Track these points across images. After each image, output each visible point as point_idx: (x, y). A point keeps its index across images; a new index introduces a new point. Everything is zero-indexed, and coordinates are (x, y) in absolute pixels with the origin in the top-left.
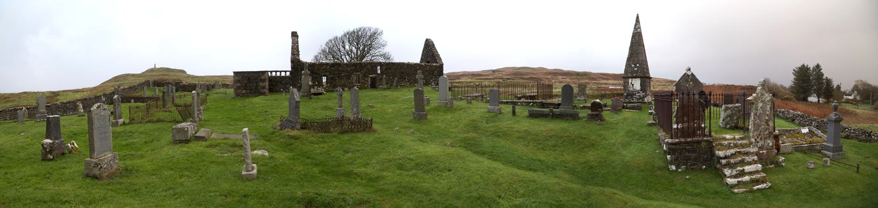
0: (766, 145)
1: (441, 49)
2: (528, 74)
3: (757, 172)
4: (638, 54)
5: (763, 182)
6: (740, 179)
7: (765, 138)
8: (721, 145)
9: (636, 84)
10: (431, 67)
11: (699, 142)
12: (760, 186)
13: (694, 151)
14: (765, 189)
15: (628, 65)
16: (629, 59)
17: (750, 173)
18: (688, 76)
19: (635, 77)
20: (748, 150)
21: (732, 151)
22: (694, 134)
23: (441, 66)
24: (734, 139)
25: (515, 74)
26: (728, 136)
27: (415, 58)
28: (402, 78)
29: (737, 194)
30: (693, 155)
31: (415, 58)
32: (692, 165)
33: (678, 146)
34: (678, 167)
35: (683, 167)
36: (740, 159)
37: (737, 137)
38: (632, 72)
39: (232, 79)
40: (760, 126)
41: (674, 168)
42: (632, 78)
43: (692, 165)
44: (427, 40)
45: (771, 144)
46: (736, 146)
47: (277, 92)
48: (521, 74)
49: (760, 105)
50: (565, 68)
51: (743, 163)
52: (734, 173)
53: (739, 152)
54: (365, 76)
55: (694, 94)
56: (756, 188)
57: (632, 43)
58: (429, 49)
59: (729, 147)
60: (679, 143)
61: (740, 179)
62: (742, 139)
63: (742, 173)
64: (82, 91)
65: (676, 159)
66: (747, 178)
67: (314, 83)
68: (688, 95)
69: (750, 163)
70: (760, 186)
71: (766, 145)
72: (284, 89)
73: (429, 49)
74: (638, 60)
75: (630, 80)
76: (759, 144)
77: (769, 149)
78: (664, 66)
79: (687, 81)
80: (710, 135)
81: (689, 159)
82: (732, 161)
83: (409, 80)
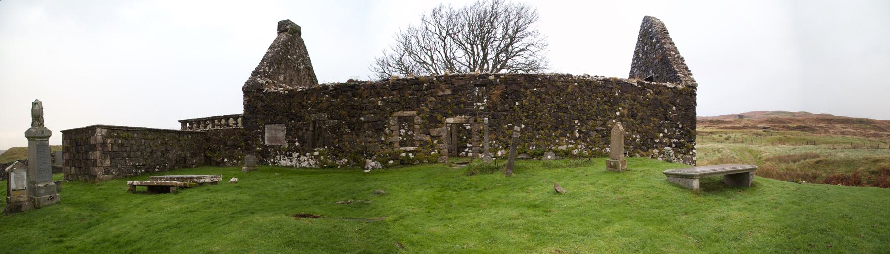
1: (686, 43)
2: (791, 121)
10: (658, 91)
23: (690, 92)
25: (772, 121)
27: (615, 62)
28: (562, 127)
31: (615, 62)
44: (647, 20)
47: (218, 164)
48: (781, 121)
50: (837, 113)
54: (433, 121)
58: (655, 48)
64: (785, 113)
67: (291, 142)
72: (231, 158)
73: (655, 48)
78: (57, 126)
83: (585, 136)
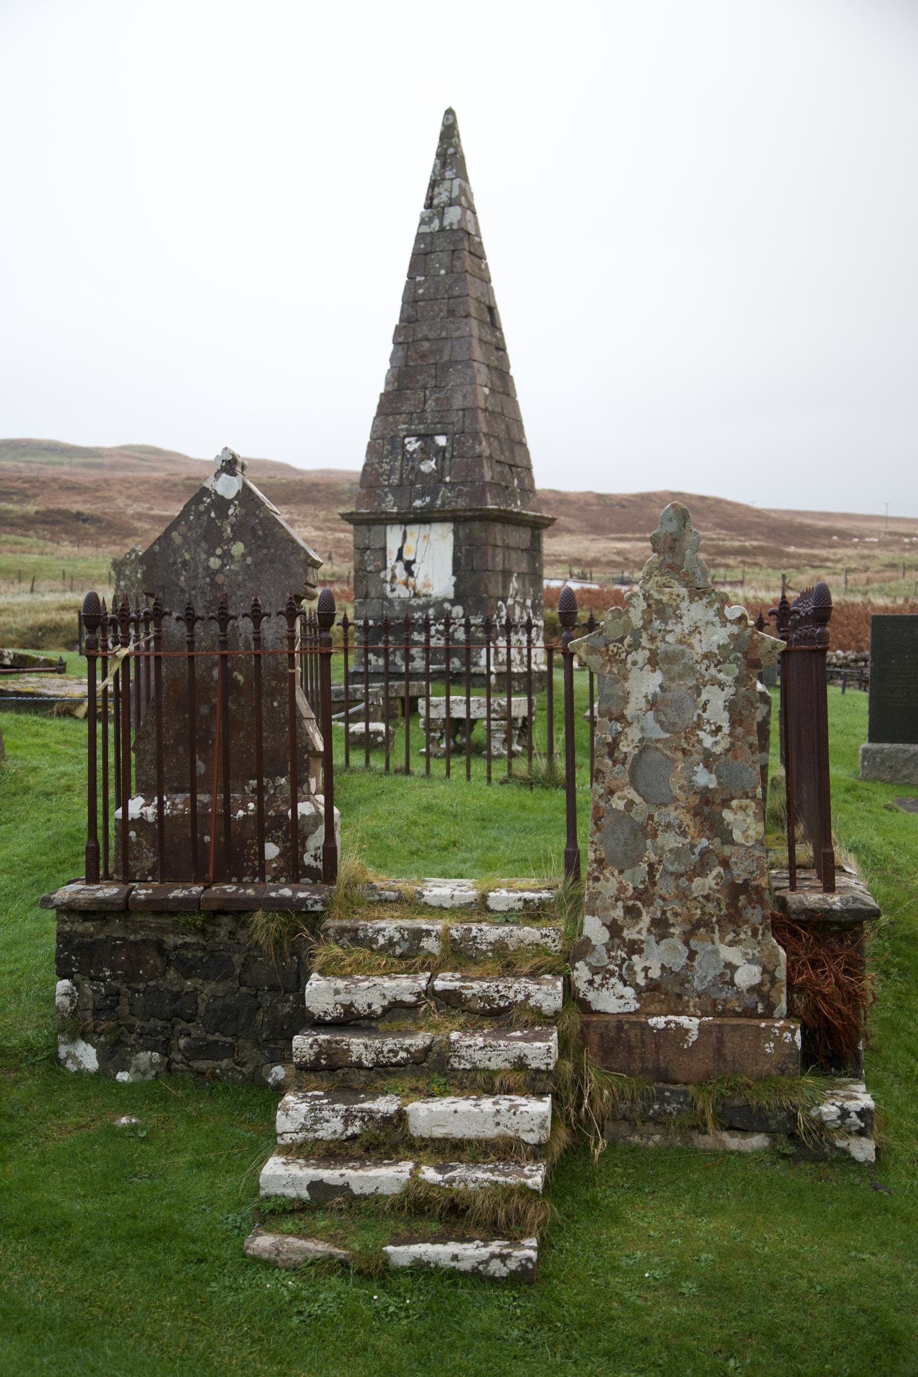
0: (704, 974)
2: (37, 486)
3: (504, 1150)
4: (443, 369)
5: (493, 1229)
6: (330, 1175)
7: (694, 929)
8: (355, 938)
9: (429, 561)
11: (239, 911)
12: (440, 1252)
13: (214, 965)
14: (477, 1277)
15: (384, 442)
16: (389, 405)
17: (449, 1150)
18: (221, 504)
19: (425, 518)
20: (517, 989)
21: (404, 986)
22: (236, 858)
24: (480, 908)
26: (441, 890)
29: (268, 1264)
30: (208, 991)
32: (199, 1051)
33: (116, 929)
34: (113, 1056)
35: (145, 1057)
36: (420, 1040)
37: (502, 897)
38: (403, 489)
39: (357, 479)
40: (646, 831)
41: (87, 1056)
42: (408, 519)
43: (199, 1051)
45: (747, 975)
46: (459, 954)
49: (646, 683)
51: (434, 1071)
52: (332, 1127)
53: (451, 1001)
55: (257, 615)
56: (401, 1254)
57: (412, 302)
59: (407, 955)
60: (125, 909)
61: (330, 1175)
62: (533, 912)
63: (389, 1139)
65: (106, 1007)
66: (387, 1177)
68: (224, 619)
69: (483, 1083)
70: (440, 1252)
71: (704, 974)
74: (444, 408)
75: (393, 537)
76: (652, 962)
77: (734, 1013)
79: (213, 538)
80: (328, 871)
81: (179, 1010)
82: (358, 1046)
